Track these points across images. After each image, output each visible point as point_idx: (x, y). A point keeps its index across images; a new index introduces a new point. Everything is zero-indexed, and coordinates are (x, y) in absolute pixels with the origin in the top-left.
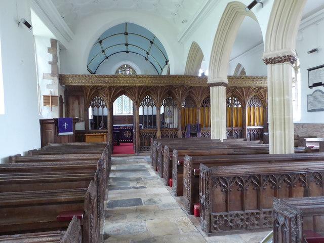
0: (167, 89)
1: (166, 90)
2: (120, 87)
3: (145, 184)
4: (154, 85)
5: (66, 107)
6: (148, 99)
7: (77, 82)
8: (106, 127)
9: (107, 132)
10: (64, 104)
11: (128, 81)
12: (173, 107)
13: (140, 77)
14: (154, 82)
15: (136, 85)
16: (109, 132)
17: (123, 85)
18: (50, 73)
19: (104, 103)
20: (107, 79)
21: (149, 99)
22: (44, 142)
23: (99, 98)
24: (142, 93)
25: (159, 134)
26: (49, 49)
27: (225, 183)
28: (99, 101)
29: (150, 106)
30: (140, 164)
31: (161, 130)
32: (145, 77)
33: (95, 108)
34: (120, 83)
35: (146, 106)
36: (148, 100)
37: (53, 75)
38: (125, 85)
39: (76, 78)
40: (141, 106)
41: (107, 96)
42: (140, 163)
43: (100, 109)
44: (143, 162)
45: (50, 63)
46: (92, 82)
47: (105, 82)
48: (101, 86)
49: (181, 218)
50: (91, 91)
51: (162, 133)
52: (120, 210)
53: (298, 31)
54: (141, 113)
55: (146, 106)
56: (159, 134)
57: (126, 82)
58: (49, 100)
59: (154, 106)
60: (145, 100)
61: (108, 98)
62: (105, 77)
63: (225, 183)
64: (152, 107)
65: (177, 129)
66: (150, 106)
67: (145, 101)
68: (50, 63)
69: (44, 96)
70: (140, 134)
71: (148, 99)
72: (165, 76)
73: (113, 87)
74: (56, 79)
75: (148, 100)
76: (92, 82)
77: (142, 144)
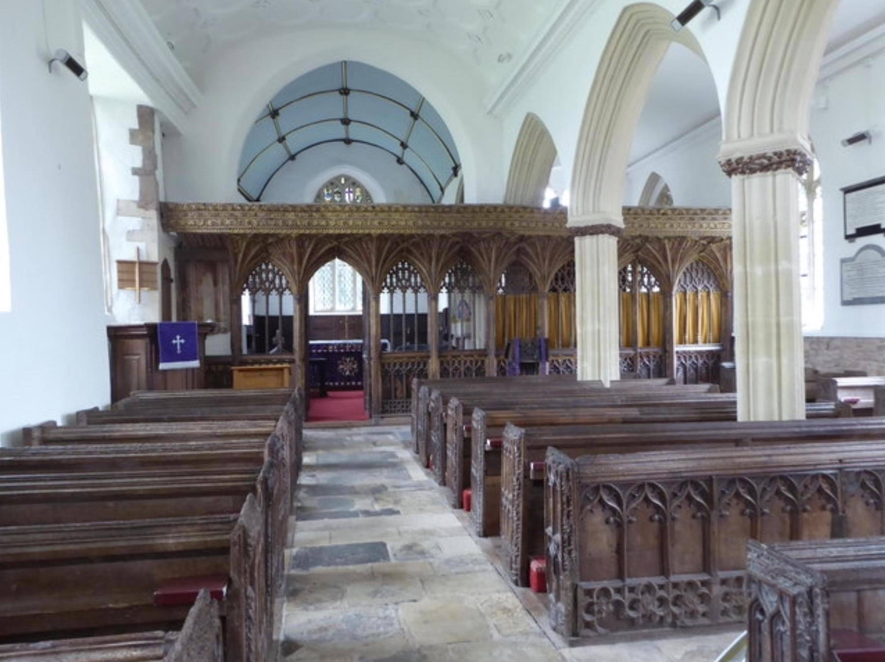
7: (209, 222)
8: (288, 347)
10: (173, 286)
11: (351, 222)
37: (143, 204)
42: (381, 445)
45: (135, 172)
49: (495, 596)
68: (135, 172)
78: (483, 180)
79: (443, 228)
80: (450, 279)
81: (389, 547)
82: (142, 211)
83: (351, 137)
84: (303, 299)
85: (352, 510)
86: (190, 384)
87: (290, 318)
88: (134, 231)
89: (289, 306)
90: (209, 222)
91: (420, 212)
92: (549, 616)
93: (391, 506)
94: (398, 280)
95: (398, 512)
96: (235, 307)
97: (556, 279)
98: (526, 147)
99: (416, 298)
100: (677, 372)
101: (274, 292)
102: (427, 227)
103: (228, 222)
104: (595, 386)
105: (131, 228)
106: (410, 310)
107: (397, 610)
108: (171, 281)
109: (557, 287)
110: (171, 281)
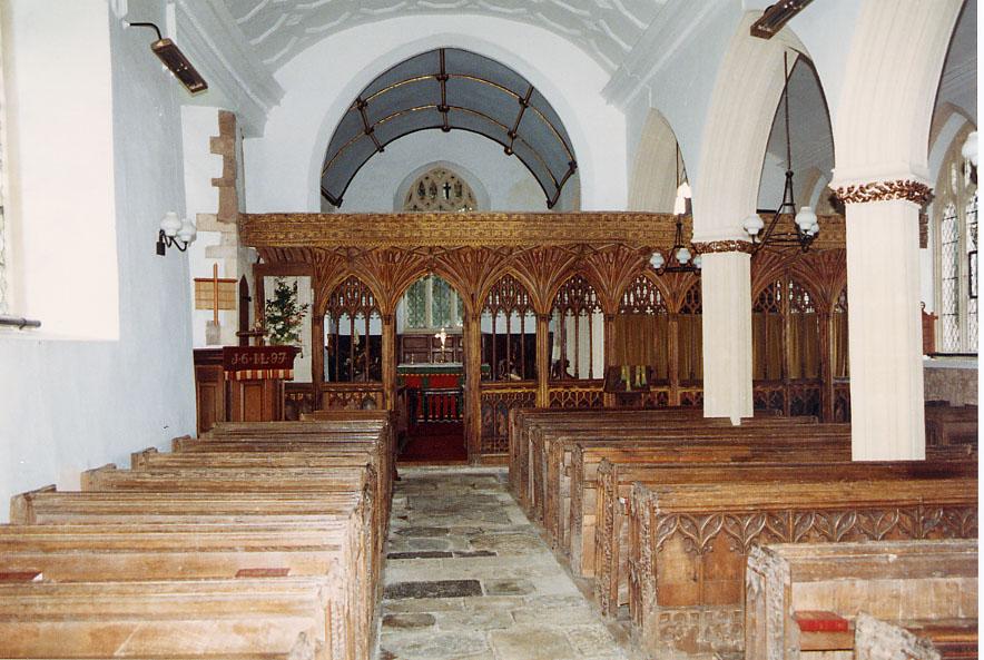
3: (492, 546)
5: (827, 360)
7: (291, 236)
8: (376, 375)
10: (252, 304)
11: (448, 234)
18: (217, 212)
22: (203, 425)
26: (213, 141)
27: (854, 657)
30: (482, 491)
36: (642, 290)
37: (222, 217)
42: (481, 487)
44: (491, 486)
45: (215, 182)
49: (583, 626)
52: (326, 23)
53: (948, 103)
58: (211, 286)
63: (854, 657)
68: (215, 182)
69: (196, 280)
74: (232, 227)
78: (605, 186)
79: (555, 239)
80: (590, 298)
81: (482, 584)
82: (221, 224)
83: (450, 124)
84: (389, 319)
85: (446, 551)
86: (268, 411)
87: (379, 338)
88: (213, 247)
89: (376, 327)
90: (291, 236)
91: (528, 220)
92: (565, 558)
93: (486, 549)
94: (501, 299)
95: (494, 554)
96: (317, 328)
97: (689, 297)
98: (85, 513)
99: (523, 322)
100: (836, 408)
101: (360, 316)
102: (535, 238)
103: (311, 235)
104: (721, 425)
105: (210, 244)
106: (516, 330)
107: (486, 635)
108: (250, 299)
109: (690, 306)
110: (250, 299)
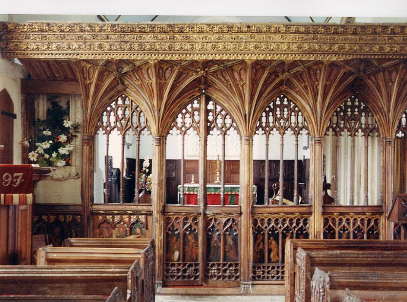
0: (350, 73)
1: (347, 75)
2: (193, 63)
4: (305, 58)
6: (282, 107)
7: (54, 46)
9: (149, 214)
11: (221, 46)
12: (366, 136)
13: (260, 32)
14: (306, 46)
15: (247, 58)
16: (156, 215)
17: (204, 58)
19: (142, 119)
20: (149, 37)
21: (287, 106)
23: (127, 102)
24: (266, 84)
25: (316, 225)
28: (128, 113)
29: (289, 132)
31: (324, 213)
32: (277, 32)
33: (130, 137)
34: (191, 51)
35: (345, 133)
36: (282, 111)
38: (210, 58)
39: (50, 35)
40: (260, 131)
41: (151, 96)
43: (215, 137)
46: (100, 46)
47: (142, 48)
48: (127, 62)
50: (101, 79)
51: (326, 222)
54: (258, 154)
55: (345, 133)
56: (316, 225)
57: (214, 47)
59: (304, 132)
60: (273, 111)
61: (155, 103)
62: (143, 31)
64: (297, 134)
65: (378, 211)
66: (289, 132)
67: (274, 115)
70: (255, 222)
71: (282, 107)
72: (67, 137)
73: (171, 64)
75: (282, 111)
76: (100, 46)
77: (259, 258)
